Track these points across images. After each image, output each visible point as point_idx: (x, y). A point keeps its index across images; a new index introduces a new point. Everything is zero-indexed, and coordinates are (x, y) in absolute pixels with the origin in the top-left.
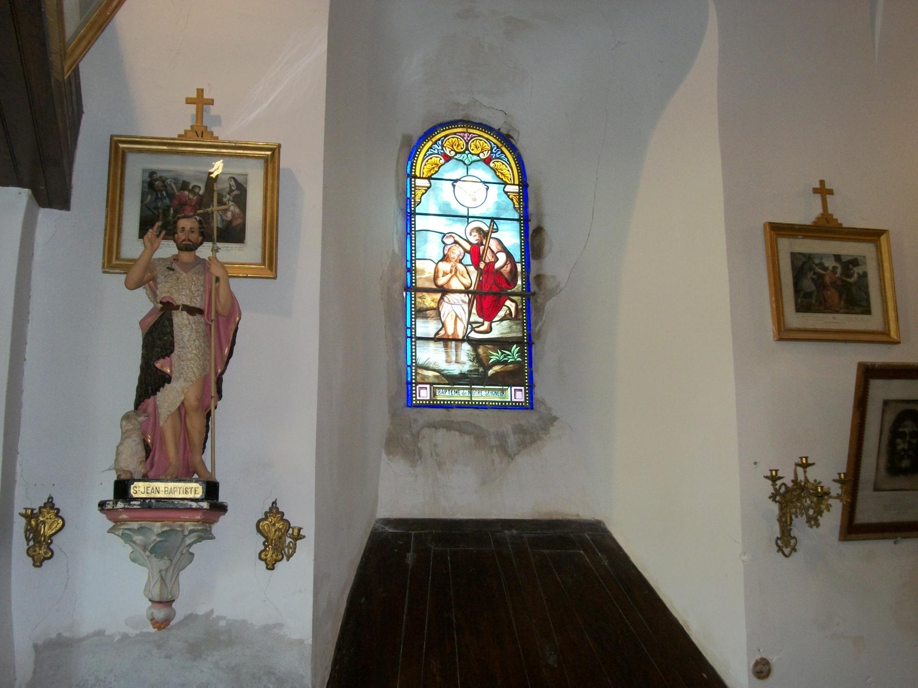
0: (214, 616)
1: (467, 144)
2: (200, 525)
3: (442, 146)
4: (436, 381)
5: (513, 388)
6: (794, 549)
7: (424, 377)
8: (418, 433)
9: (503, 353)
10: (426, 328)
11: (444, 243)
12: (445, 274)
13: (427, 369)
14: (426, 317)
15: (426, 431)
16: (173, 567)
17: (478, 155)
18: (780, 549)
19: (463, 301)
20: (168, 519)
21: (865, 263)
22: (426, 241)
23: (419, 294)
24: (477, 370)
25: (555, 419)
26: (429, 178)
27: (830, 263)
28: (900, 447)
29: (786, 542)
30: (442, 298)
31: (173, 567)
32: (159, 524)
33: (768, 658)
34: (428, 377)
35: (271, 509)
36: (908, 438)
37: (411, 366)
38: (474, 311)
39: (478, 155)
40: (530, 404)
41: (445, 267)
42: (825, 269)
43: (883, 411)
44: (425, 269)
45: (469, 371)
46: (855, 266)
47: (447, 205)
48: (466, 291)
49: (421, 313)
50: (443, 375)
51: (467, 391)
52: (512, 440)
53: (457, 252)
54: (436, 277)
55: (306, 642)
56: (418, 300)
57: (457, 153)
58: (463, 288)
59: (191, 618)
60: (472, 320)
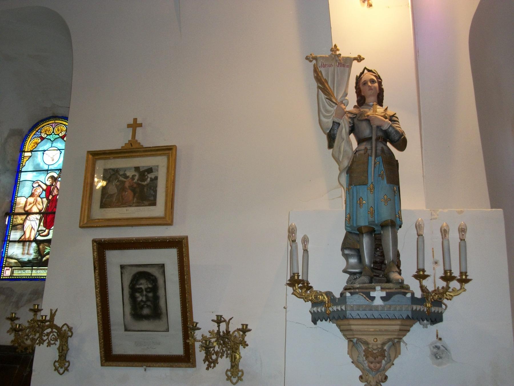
1: (54, 129)
3: (41, 132)
6: (67, 369)
7: (10, 263)
10: (15, 235)
11: (33, 186)
12: (30, 204)
14: (16, 229)
17: (58, 135)
19: (37, 219)
21: (157, 170)
22: (24, 187)
23: (15, 217)
24: (37, 258)
26: (31, 151)
27: (130, 174)
28: (140, 299)
30: (26, 218)
34: (11, 263)
36: (144, 293)
38: (42, 224)
39: (58, 135)
41: (31, 200)
42: (126, 177)
43: (122, 273)
44: (21, 201)
45: (33, 259)
46: (148, 173)
47: (38, 165)
48: (40, 213)
49: (15, 227)
51: (30, 271)
54: (25, 206)
56: (14, 220)
57: (48, 135)
58: (38, 211)
60: (40, 229)
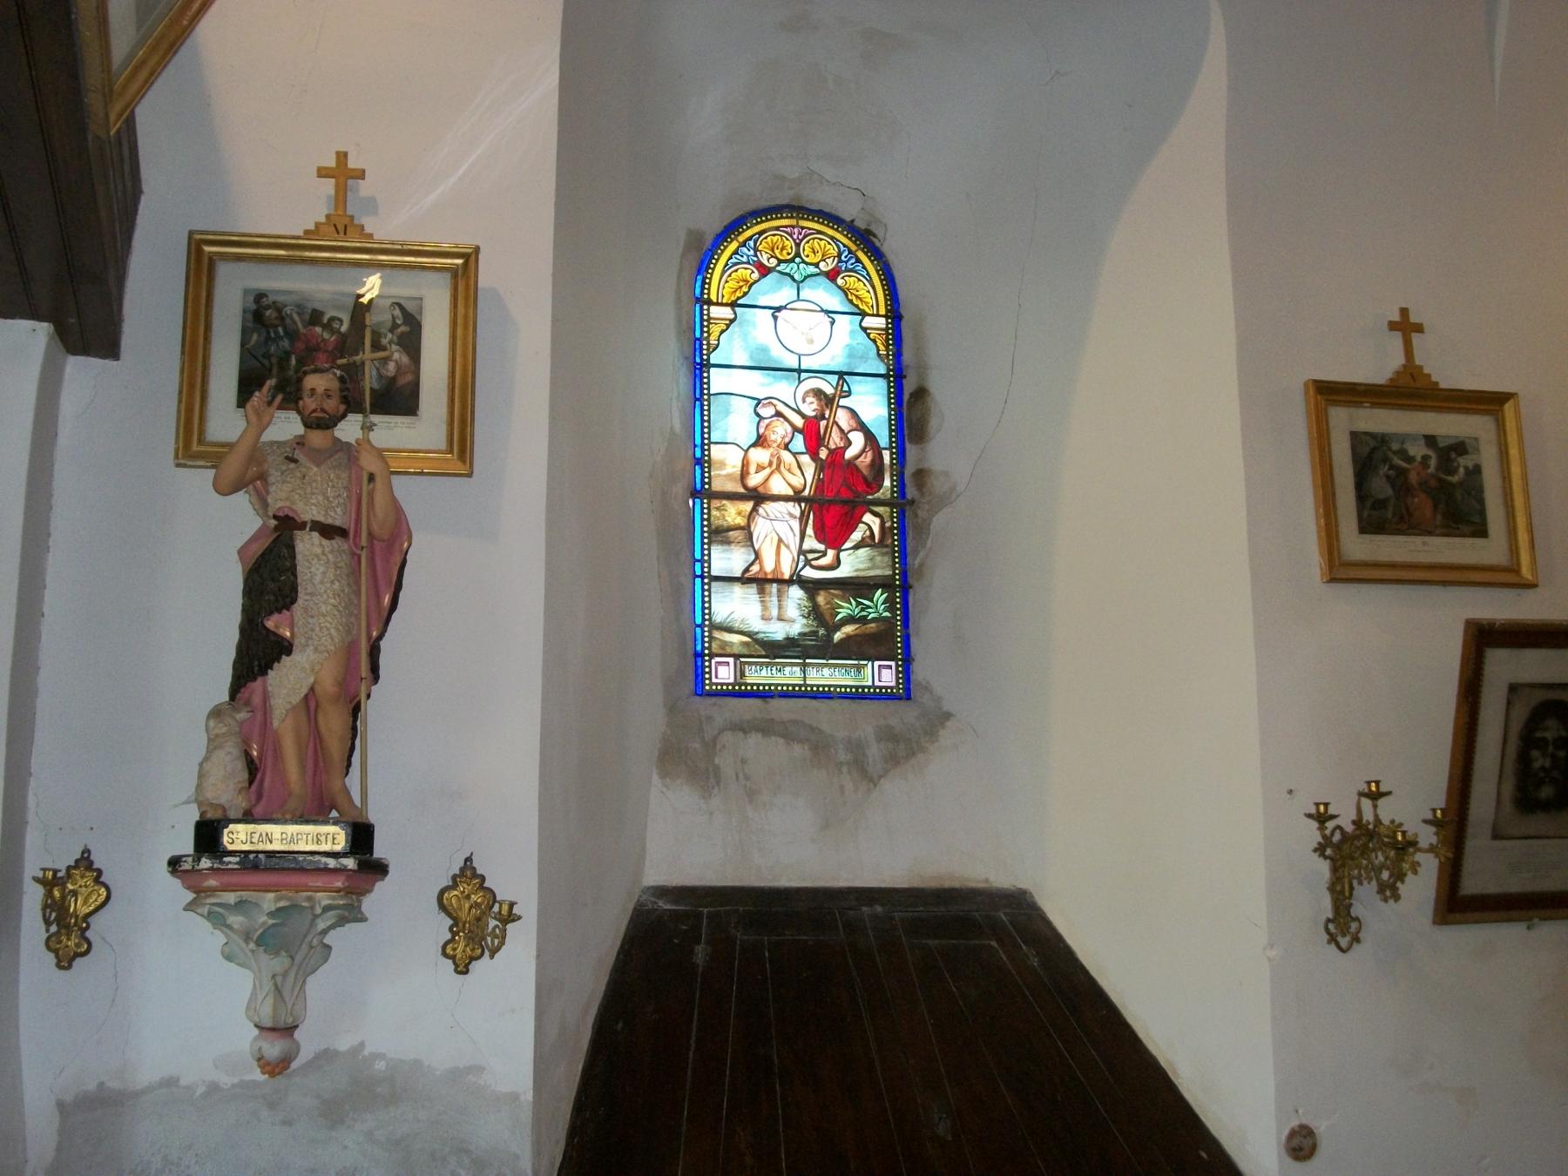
0: (366, 1052)
1: (798, 245)
2: (341, 898)
3: (756, 250)
4: (745, 651)
5: (877, 663)
6: (1356, 939)
7: (725, 644)
8: (714, 740)
9: (859, 604)
10: (727, 560)
11: (758, 415)
12: (760, 468)
13: (730, 630)
14: (728, 542)
15: (728, 737)
16: (295, 968)
17: (817, 265)
18: (1332, 939)
19: (791, 515)
20: (287, 887)
21: (1478, 450)
22: (727, 413)
23: (716, 503)
24: (815, 633)
25: (948, 716)
26: (733, 305)
27: (1417, 450)
28: (1537, 765)
29: (1342, 926)
30: (754, 509)
31: (295, 968)
32: (271, 895)
33: (1313, 1124)
34: (731, 644)
35: (462, 870)
36: (1551, 749)
37: (701, 626)
38: (810, 531)
39: (817, 265)
40: (905, 691)
41: (759, 456)
42: (1410, 459)
43: (1509, 703)
44: (726, 460)
45: (802, 634)
46: (1461, 454)
47: (764, 350)
48: (797, 497)
49: (719, 534)
50: (756, 641)
51: (797, 669)
52: (874, 752)
54: (744, 474)
55: (522, 1098)
56: (714, 513)
57: (780, 262)
58: (791, 493)
59: (326, 1056)
60: (806, 546)
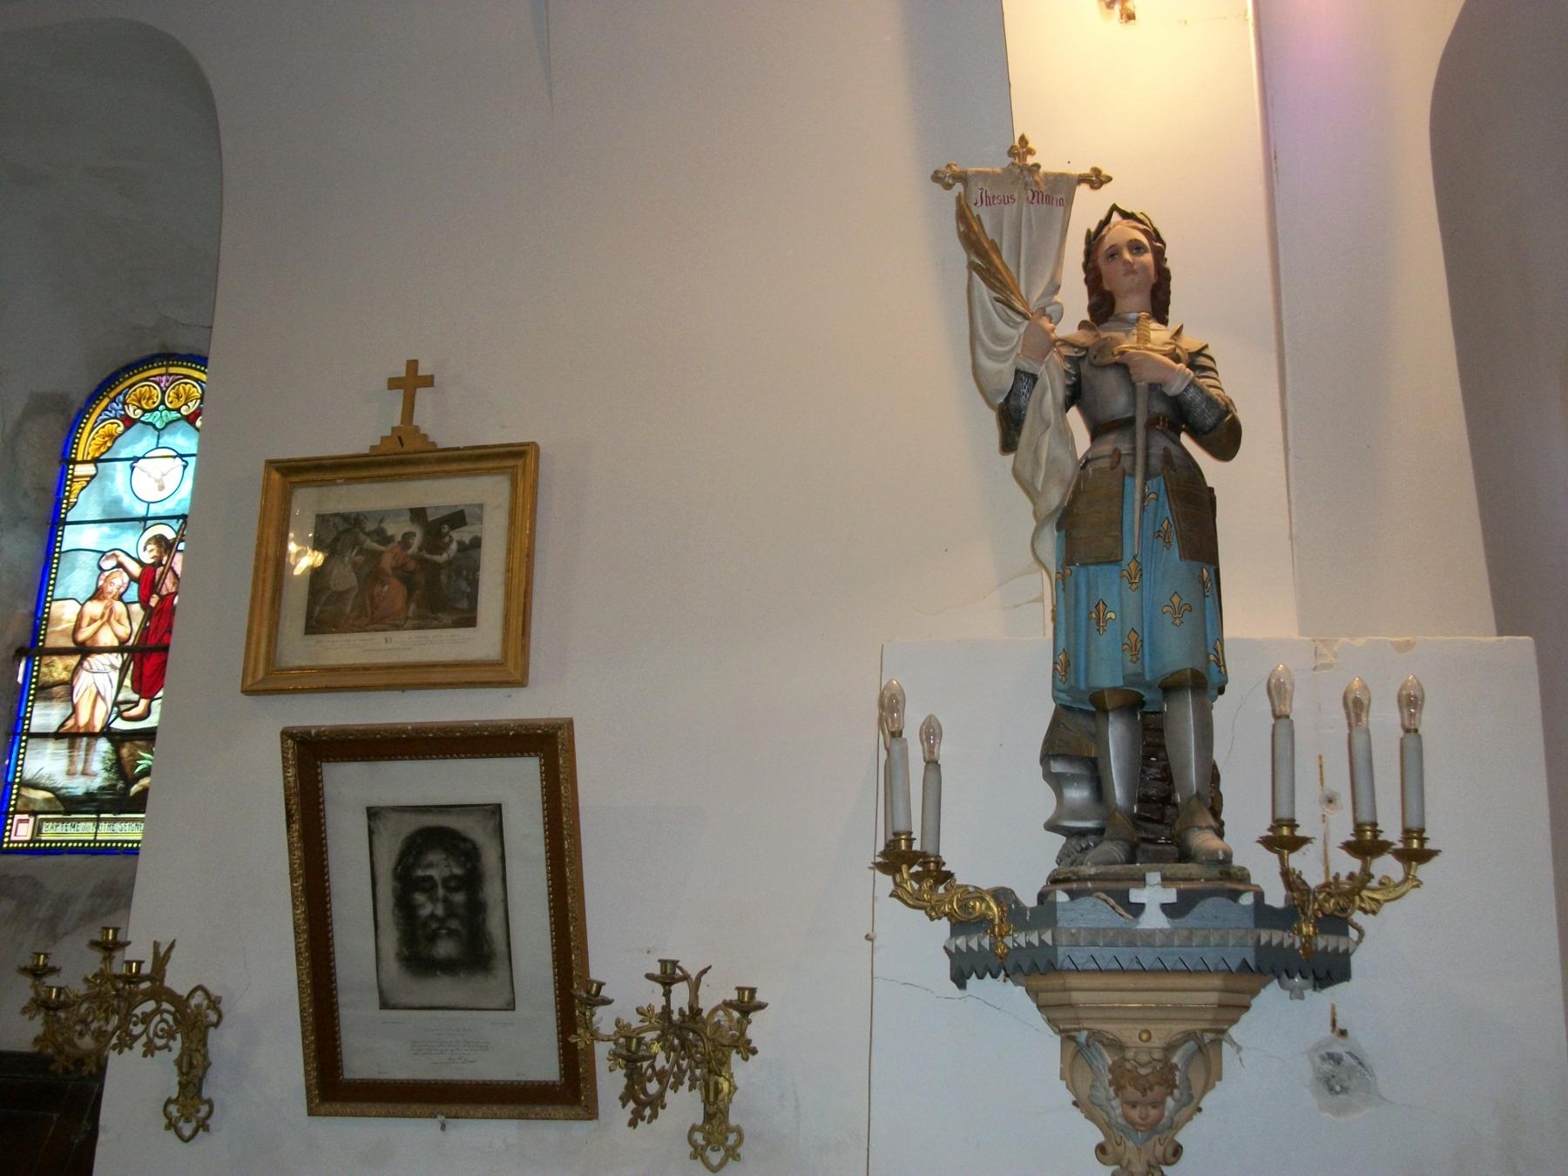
1: (163, 393)
3: (124, 403)
6: (203, 1125)
10: (45, 716)
11: (100, 568)
12: (93, 621)
14: (50, 698)
17: (178, 410)
19: (113, 667)
21: (480, 519)
22: (73, 568)
23: (46, 660)
24: (112, 787)
26: (96, 461)
27: (395, 529)
28: (426, 911)
30: (80, 664)
34: (33, 801)
36: (441, 892)
38: (127, 682)
39: (178, 410)
41: (95, 608)
42: (385, 539)
43: (371, 833)
44: (63, 613)
45: (101, 788)
46: (453, 527)
47: (117, 502)
48: (121, 648)
49: (45, 691)
51: (90, 824)
53: (120, 579)
54: (77, 627)
56: (44, 669)
57: (145, 411)
58: (116, 643)
60: (121, 697)
